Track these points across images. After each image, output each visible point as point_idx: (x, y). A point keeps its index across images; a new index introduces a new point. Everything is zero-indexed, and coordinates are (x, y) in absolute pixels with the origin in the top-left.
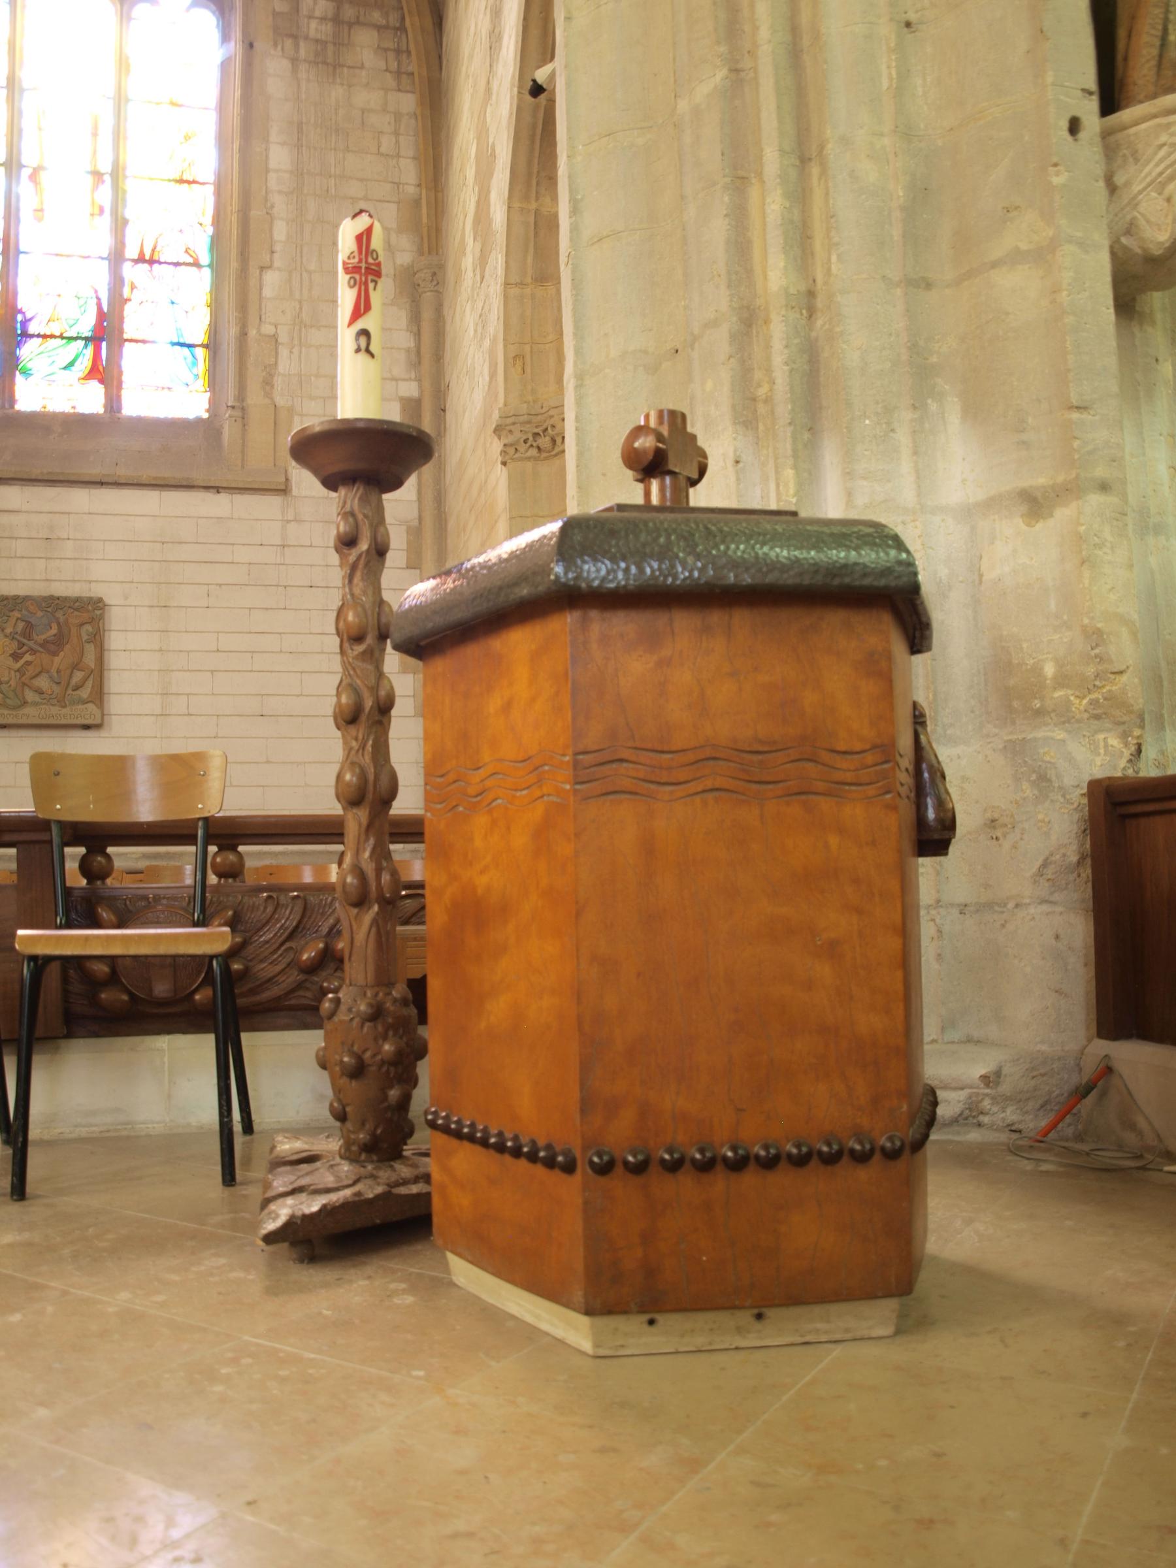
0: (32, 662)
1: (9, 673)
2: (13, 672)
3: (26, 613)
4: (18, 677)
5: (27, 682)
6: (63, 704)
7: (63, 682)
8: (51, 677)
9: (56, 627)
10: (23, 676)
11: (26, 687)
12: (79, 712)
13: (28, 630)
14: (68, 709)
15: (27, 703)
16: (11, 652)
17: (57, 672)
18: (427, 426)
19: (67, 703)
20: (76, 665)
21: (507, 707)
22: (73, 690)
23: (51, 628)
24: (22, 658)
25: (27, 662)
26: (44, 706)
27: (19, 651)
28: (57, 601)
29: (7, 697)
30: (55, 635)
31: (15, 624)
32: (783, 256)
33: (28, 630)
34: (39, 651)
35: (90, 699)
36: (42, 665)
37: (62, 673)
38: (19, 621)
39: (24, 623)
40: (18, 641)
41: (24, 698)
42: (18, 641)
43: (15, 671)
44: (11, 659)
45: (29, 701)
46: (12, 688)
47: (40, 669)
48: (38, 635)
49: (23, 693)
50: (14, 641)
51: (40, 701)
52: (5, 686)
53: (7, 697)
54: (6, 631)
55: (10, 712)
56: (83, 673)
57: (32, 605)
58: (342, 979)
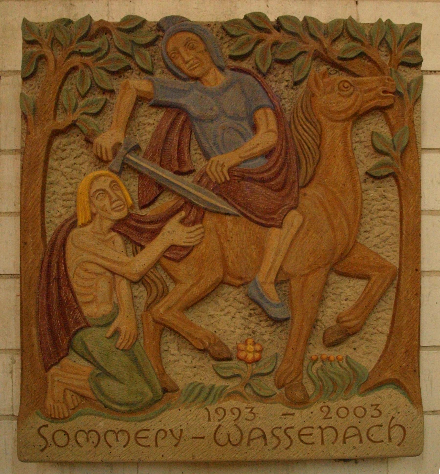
0: (190, 249)
1: (113, 288)
2: (123, 286)
3: (169, 79)
4: (142, 302)
5: (170, 318)
6: (298, 395)
7: (297, 318)
8: (253, 301)
9: (273, 125)
10: (156, 300)
11: (168, 337)
12: (352, 420)
13: (175, 138)
14: (316, 408)
15: (176, 390)
16: (117, 216)
17: (277, 283)
18: (156, 23)
19: (310, 388)
20: (343, 257)
21: (340, 108)
22: (330, 345)
23: (255, 128)
24: (155, 233)
25: (172, 247)
26: (233, 403)
27: (146, 212)
28: (276, 35)
29: (108, 374)
30: (267, 154)
31: (132, 117)
32: (138, 30)
33: (175, 138)
34: (217, 212)
35: (388, 375)
36: (224, 260)
37: (295, 285)
38: (144, 109)
39: (162, 113)
40: (141, 175)
41: (162, 373)
42: (141, 175)
43: (132, 283)
44: (119, 240)
45: (181, 384)
46: (121, 342)
47: (219, 273)
48: (207, 156)
49: (160, 357)
50: (127, 175)
51: (221, 383)
52: (99, 333)
53: (108, 374)
54: (98, 140)
55: (117, 425)
56: (361, 285)
57: (188, 46)
58: (326, 307)
